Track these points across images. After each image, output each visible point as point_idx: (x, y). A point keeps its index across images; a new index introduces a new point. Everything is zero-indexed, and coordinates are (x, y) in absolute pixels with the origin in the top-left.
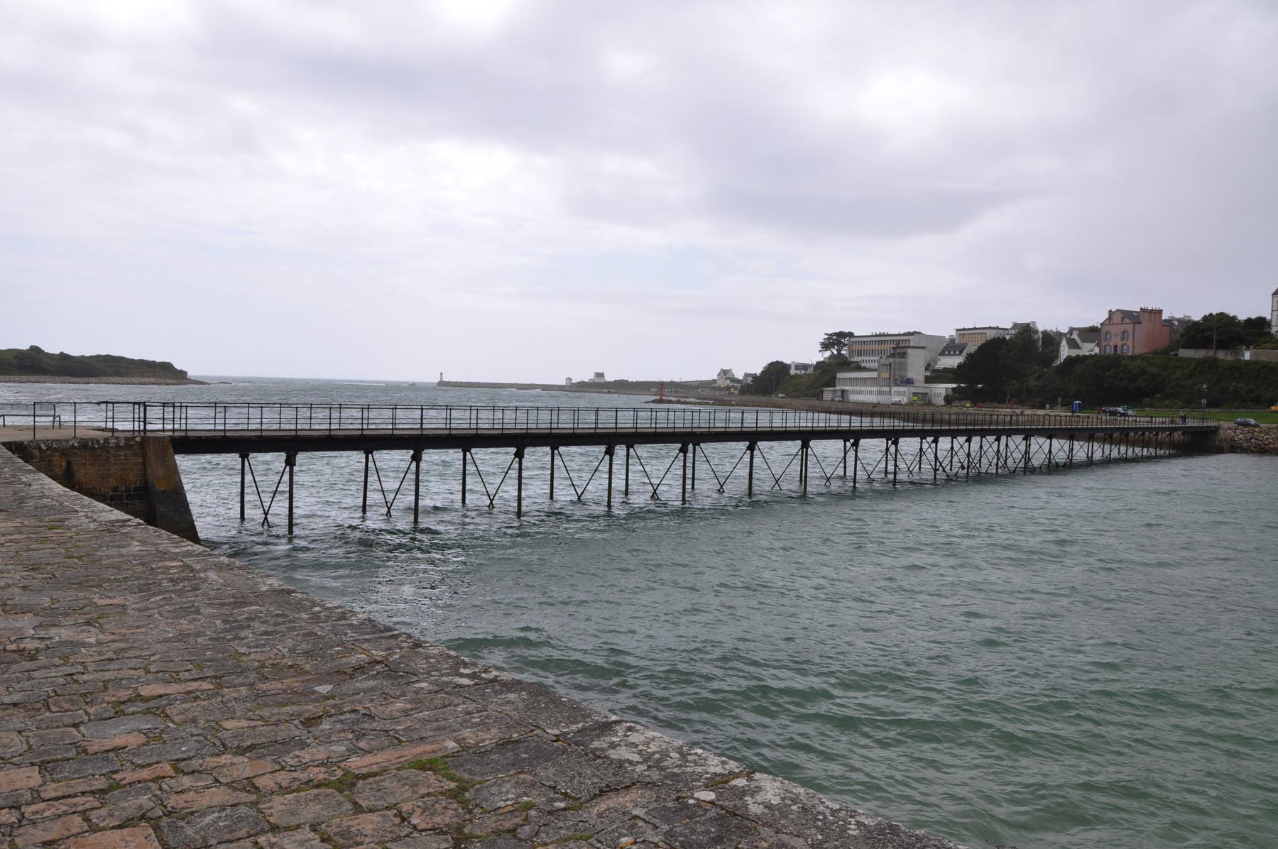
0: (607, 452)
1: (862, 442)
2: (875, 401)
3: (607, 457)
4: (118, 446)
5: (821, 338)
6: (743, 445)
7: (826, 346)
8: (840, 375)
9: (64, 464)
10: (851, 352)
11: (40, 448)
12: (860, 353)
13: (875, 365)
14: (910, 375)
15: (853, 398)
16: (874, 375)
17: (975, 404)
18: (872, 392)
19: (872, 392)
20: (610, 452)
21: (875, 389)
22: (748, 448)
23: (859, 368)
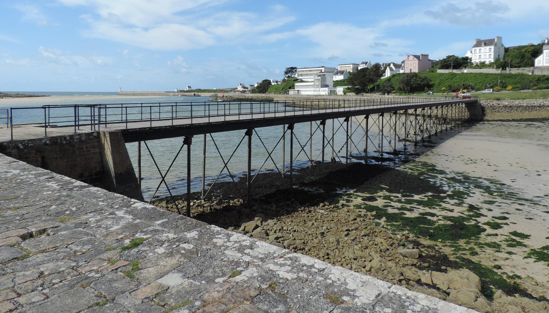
0: (185, 142)
1: (296, 125)
2: (411, 96)
3: (186, 146)
4: (80, 141)
5: (285, 70)
6: (180, 140)
7: (286, 73)
8: (296, 84)
9: (39, 159)
10: (298, 75)
11: (18, 148)
12: (302, 75)
13: (313, 80)
14: (327, 83)
15: (302, 93)
16: (312, 83)
17: (388, 94)
18: (311, 91)
19: (311, 91)
20: (187, 142)
21: (313, 89)
22: (247, 134)
23: (302, 81)
